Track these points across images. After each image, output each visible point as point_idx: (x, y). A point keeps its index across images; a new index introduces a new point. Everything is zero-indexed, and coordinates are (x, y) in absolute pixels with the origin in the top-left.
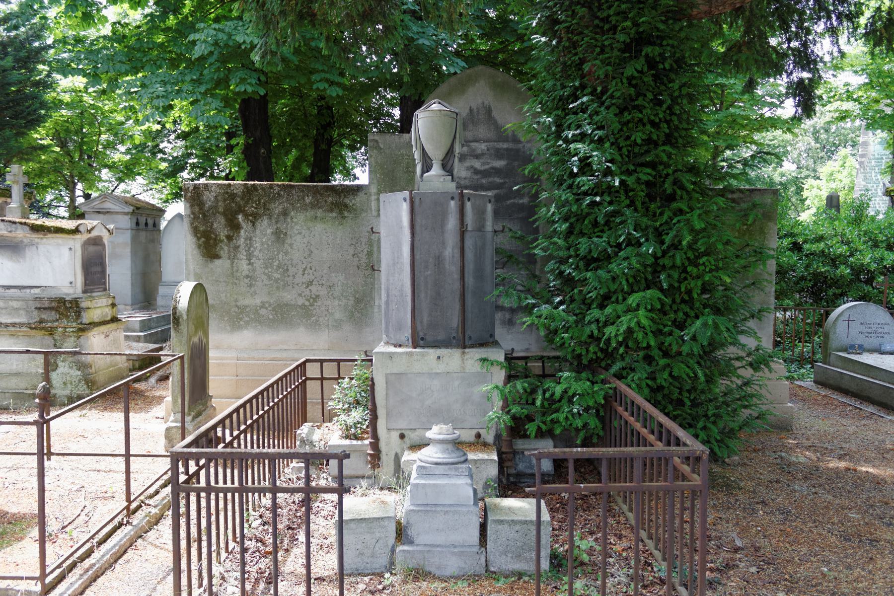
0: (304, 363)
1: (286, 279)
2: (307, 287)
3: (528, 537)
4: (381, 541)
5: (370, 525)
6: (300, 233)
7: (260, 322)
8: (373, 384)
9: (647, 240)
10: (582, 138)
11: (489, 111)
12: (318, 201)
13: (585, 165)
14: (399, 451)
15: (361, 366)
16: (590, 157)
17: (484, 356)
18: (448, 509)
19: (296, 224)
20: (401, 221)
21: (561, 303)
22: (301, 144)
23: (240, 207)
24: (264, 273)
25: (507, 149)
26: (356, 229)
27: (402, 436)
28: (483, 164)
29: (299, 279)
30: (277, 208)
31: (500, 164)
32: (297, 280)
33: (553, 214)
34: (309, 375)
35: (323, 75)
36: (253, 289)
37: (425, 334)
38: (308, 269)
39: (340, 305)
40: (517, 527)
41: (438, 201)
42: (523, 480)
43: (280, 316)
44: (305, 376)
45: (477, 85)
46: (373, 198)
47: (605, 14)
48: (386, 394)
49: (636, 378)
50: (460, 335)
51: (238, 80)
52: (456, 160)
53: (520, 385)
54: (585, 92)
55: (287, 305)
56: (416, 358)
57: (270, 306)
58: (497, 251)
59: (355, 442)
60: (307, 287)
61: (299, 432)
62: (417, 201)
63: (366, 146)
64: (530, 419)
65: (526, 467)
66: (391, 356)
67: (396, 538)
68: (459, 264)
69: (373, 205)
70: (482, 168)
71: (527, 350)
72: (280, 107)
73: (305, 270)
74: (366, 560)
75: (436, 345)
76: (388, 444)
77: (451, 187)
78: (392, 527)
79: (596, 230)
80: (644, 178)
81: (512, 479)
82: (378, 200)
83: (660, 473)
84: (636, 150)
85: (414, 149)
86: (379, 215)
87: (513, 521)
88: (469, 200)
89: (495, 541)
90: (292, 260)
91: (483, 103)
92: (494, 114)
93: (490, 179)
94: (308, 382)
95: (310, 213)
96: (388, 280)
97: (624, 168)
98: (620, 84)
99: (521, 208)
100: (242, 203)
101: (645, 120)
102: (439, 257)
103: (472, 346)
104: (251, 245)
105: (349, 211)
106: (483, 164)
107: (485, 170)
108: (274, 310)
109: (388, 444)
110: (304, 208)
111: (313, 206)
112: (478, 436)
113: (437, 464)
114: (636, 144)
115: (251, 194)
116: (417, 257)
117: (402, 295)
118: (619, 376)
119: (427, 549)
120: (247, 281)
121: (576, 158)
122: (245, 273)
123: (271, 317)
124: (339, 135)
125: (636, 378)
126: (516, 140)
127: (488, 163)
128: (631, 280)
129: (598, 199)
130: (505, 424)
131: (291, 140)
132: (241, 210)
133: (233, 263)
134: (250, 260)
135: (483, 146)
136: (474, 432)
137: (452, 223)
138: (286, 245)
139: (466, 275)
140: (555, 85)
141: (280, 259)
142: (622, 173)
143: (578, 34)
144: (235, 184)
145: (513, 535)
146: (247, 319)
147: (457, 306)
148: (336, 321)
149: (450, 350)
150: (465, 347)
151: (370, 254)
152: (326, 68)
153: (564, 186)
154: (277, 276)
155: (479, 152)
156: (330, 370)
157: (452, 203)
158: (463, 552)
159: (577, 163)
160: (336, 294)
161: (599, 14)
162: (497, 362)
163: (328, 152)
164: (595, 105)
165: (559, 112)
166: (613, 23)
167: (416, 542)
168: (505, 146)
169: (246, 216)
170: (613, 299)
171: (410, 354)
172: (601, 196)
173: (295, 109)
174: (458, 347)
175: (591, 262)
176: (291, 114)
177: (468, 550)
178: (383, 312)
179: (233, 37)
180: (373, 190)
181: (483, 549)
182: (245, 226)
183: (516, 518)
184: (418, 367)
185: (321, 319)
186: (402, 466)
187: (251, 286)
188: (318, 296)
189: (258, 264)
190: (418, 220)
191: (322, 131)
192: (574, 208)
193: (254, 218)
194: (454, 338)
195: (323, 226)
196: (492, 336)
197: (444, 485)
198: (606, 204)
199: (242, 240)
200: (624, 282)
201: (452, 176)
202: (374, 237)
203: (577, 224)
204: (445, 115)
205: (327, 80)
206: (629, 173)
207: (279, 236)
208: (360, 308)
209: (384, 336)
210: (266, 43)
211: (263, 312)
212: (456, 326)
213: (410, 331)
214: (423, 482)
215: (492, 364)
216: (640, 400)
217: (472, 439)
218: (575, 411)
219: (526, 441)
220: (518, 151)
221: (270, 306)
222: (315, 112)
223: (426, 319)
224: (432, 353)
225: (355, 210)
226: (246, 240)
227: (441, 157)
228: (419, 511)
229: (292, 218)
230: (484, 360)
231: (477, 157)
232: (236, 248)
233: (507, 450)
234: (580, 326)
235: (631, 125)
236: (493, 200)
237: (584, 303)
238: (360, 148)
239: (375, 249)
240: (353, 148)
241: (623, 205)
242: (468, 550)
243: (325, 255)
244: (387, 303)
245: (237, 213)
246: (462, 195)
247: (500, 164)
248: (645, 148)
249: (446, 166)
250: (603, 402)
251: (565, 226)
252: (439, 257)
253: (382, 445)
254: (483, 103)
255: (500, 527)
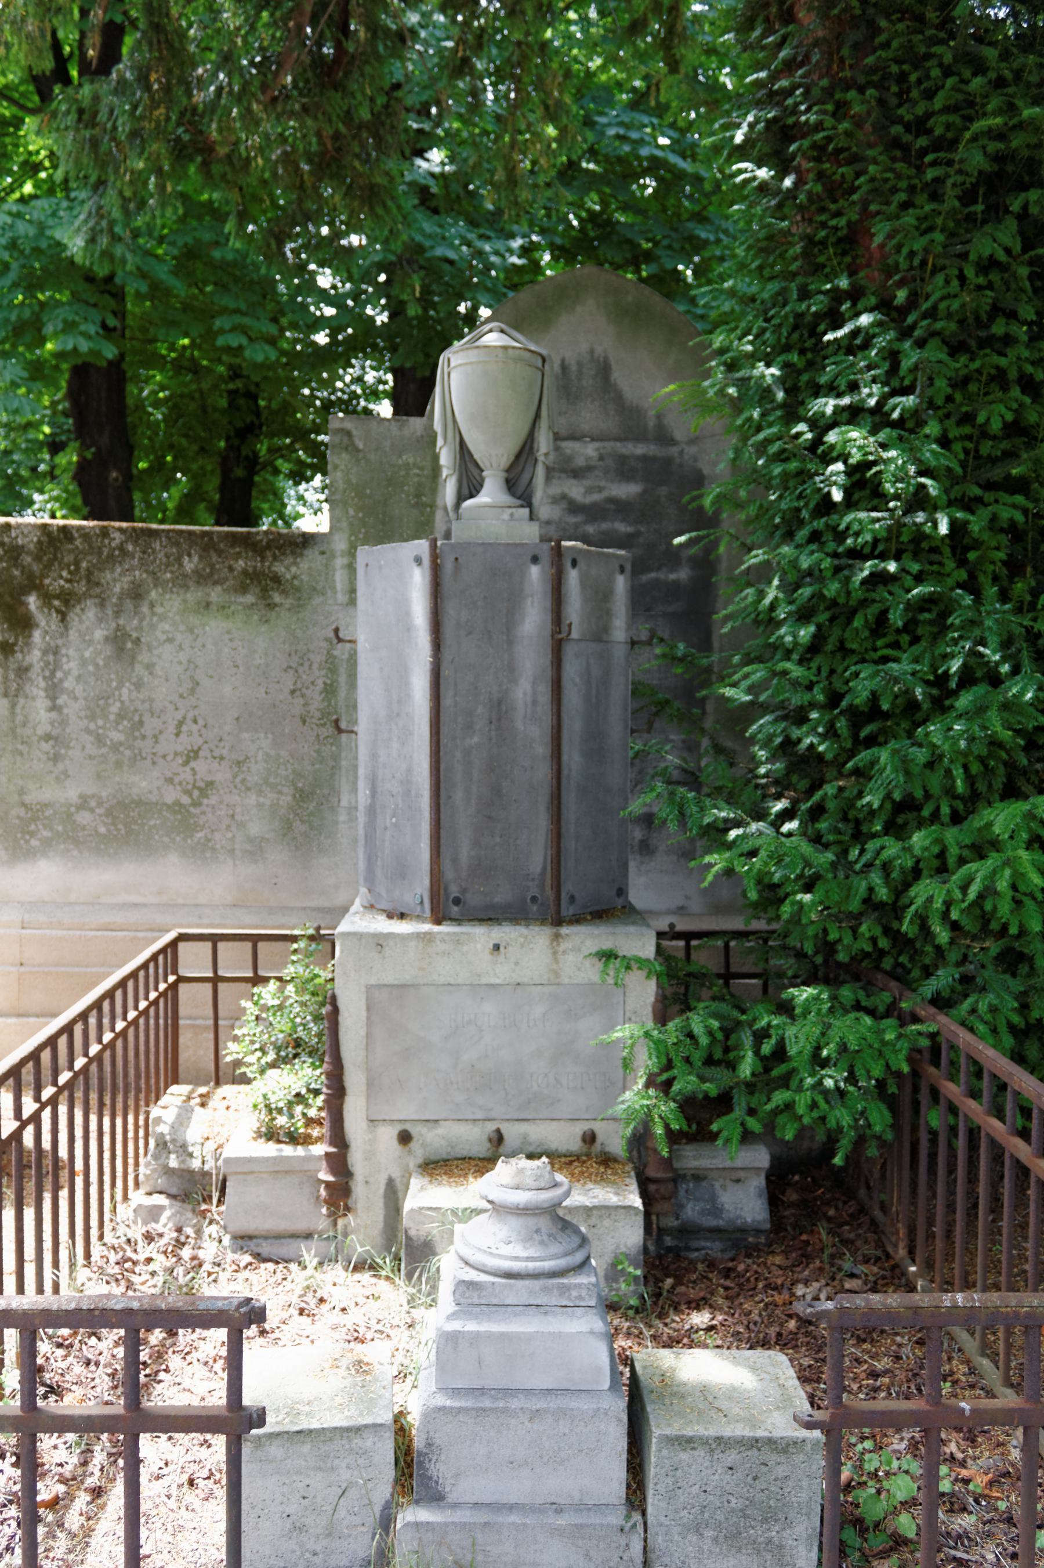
0: (174, 944)
1: (139, 743)
2: (186, 763)
3: (760, 1485)
4: (353, 1493)
5: (324, 1448)
6: (170, 640)
7: (76, 842)
8: (336, 1010)
9: (1016, 671)
10: (853, 415)
11: (604, 370)
12: (212, 566)
13: (864, 485)
14: (396, 1174)
16: (875, 463)
17: (607, 945)
18: (541, 1404)
19: (163, 618)
21: (787, 815)
22: (194, 466)
23: (31, 576)
24: (88, 731)
25: (644, 458)
27: (405, 1138)
28: (589, 490)
29: (168, 744)
30: (117, 581)
31: (626, 490)
32: (160, 749)
33: (773, 607)
34: (184, 972)
35: (238, 319)
36: (61, 766)
37: (464, 891)
38: (189, 721)
39: (260, 806)
40: (732, 1457)
41: (500, 566)
42: (695, 1244)
43: (126, 827)
44: (175, 971)
45: (579, 309)
46: (340, 562)
47: (920, 110)
48: (368, 1035)
49: (983, 1007)
50: (550, 893)
51: (60, 326)
53: (700, 1023)
54: (860, 306)
55: (139, 803)
56: (442, 947)
57: (100, 804)
59: (288, 1150)
60: (186, 763)
61: (155, 1112)
62: (448, 566)
64: (723, 1103)
65: (702, 1213)
66: (379, 941)
67: (396, 1481)
68: (548, 719)
69: (340, 578)
71: (681, 911)
72: (152, 390)
73: (181, 723)
74: (311, 1545)
75: (489, 916)
76: (369, 1156)
78: (385, 1450)
79: (879, 643)
80: (1006, 514)
81: (668, 1241)
82: (351, 568)
83: (1024, 1226)
84: (986, 448)
85: (440, 442)
86: (352, 602)
87: (719, 1439)
88: (574, 563)
89: (670, 1497)
90: (152, 700)
91: (592, 352)
92: (616, 376)
93: (605, 526)
94: (183, 988)
95: (194, 595)
96: (374, 756)
97: (956, 492)
98: (955, 283)
99: (674, 590)
100: (36, 568)
101: (1013, 374)
102: (500, 703)
103: (577, 920)
104: (57, 666)
105: (284, 593)
106: (589, 490)
107: (594, 505)
108: (109, 813)
109: (369, 1156)
110: (182, 582)
111: (203, 578)
112: (590, 1138)
113: (509, 1275)
114: (984, 434)
115: (56, 549)
116: (447, 701)
117: (407, 793)
118: (941, 1003)
119: (480, 1517)
120: (46, 746)
121: (839, 466)
122: (44, 728)
123: (102, 830)
124: (270, 450)
125: (983, 1007)
128: (975, 768)
129: (892, 567)
130: (667, 1126)
131: (175, 458)
132: (33, 584)
133: (13, 705)
134: (53, 699)
135: (589, 451)
136: (579, 1129)
137: (533, 619)
138: (138, 668)
141: (125, 697)
142: (950, 504)
143: (849, 162)
144: (19, 526)
145: (719, 1478)
146: (46, 834)
147: (543, 822)
148: (251, 840)
149: (522, 930)
150: (558, 921)
151: (330, 690)
152: (243, 307)
154: (116, 736)
155: (580, 462)
156: (234, 961)
157: (535, 571)
158: (581, 1526)
159: (841, 479)
160: (253, 779)
161: (901, 111)
163: (248, 484)
164: (891, 335)
165: (794, 357)
166: (938, 131)
167: (451, 1498)
168: (640, 450)
169: (46, 598)
170: (926, 813)
171: (426, 938)
172: (897, 558)
173: (182, 396)
174: (543, 922)
175: (870, 723)
176: (175, 406)
177: (595, 1519)
178: (361, 832)
179: (48, 233)
180: (340, 544)
181: (637, 1517)
182: (45, 621)
183: (727, 1432)
185: (217, 836)
186: (406, 1222)
187: (56, 758)
188: (210, 784)
189: (73, 709)
191: (236, 442)
192: (832, 589)
193: (64, 604)
194: (534, 899)
195: (224, 625)
196: (621, 892)
197: (530, 1337)
198: (908, 580)
199: (36, 654)
200: (958, 772)
202: (341, 651)
203: (841, 626)
204: (516, 360)
205: (244, 330)
206: (969, 505)
207: (123, 646)
208: (307, 810)
209: (363, 890)
210: (100, 208)
211: (84, 818)
213: (427, 882)
214: (472, 1326)
215: (628, 968)
216: (995, 1059)
217: (575, 1145)
218: (829, 1083)
219: (704, 1149)
220: (668, 461)
221: (100, 804)
222: (223, 403)
223: (465, 852)
224: (480, 936)
225: (298, 590)
226: (45, 652)
227: (505, 461)
228: (460, 1410)
229: (152, 606)
230: (608, 956)
231: (576, 474)
232: (23, 671)
233: (660, 1175)
234: (841, 875)
235: (973, 387)
236: (628, 567)
237: (845, 819)
238: (312, 478)
239: (342, 679)
241: (950, 582)
242: (595, 1519)
243: (227, 690)
244: (372, 811)
245: (25, 590)
248: (1005, 445)
249: (517, 484)
250: (906, 1069)
251: (805, 633)
253: (356, 1159)
254: (592, 352)
255: (684, 1456)
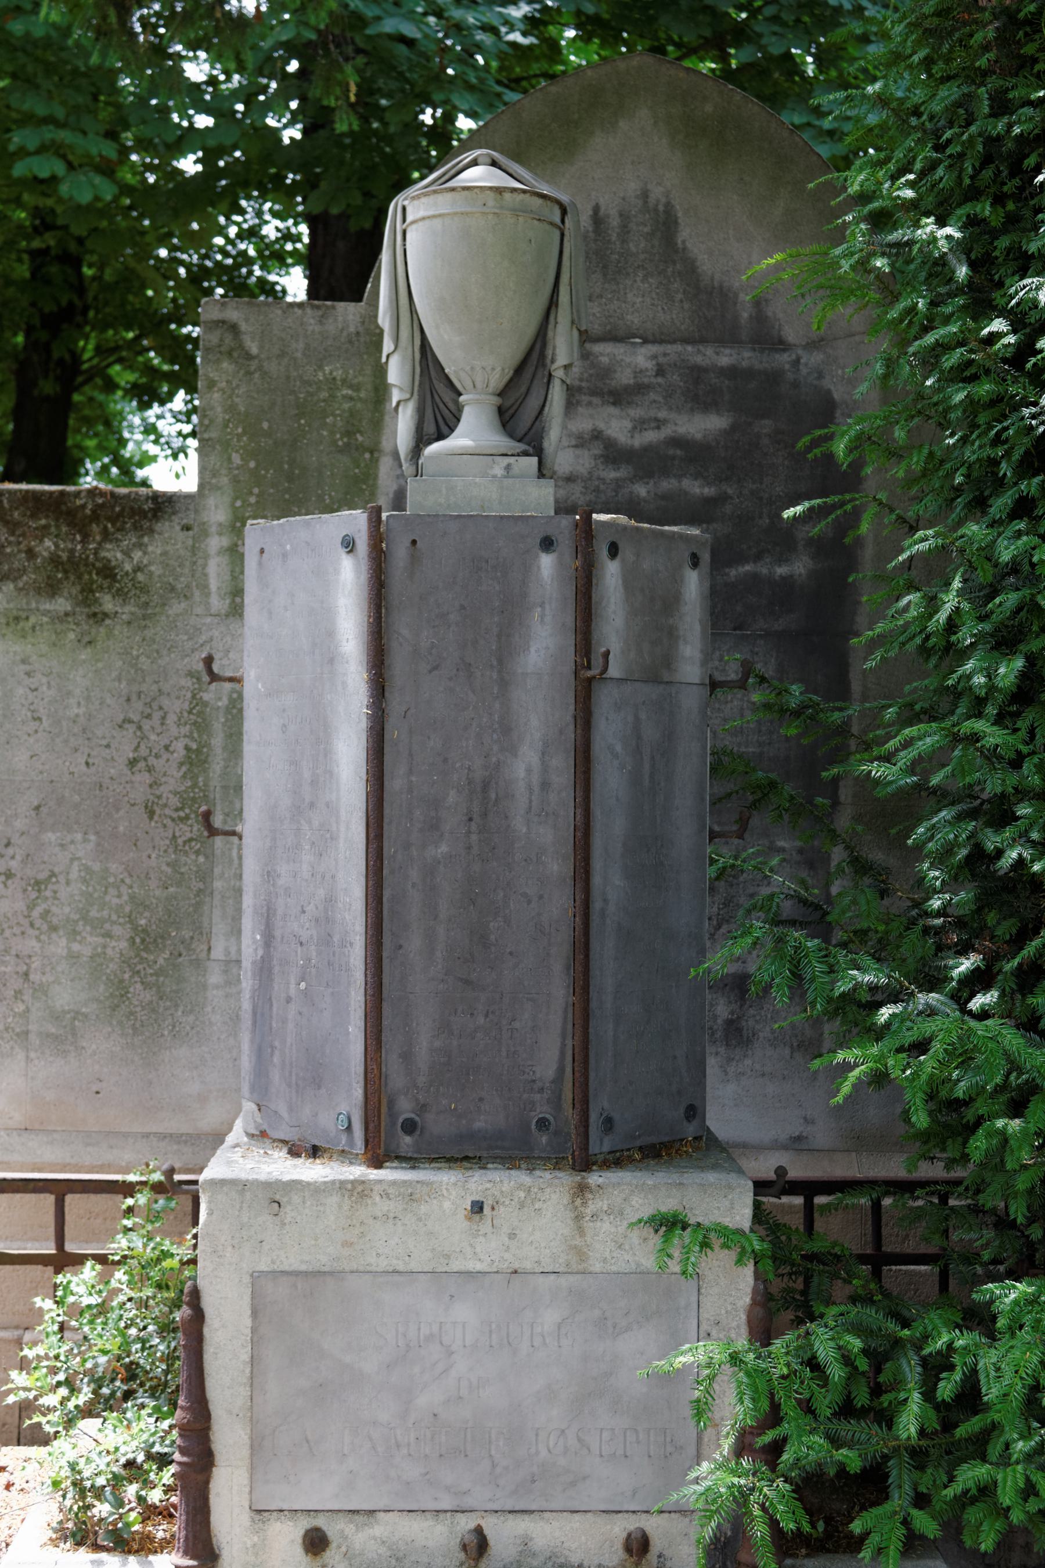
8: (198, 1316)
11: (666, 224)
15: (152, 1216)
17: (668, 1204)
20: (331, 633)
21: (978, 981)
25: (732, 372)
26: (144, 663)
28: (640, 425)
31: (702, 425)
33: (952, 626)
35: (49, 133)
37: (423, 1108)
39: (73, 957)
41: (488, 552)
46: (215, 543)
50: (569, 1113)
52: (557, 395)
56: (382, 1206)
58: (720, 765)
62: (400, 553)
63: (191, 390)
66: (275, 1196)
68: (567, 815)
69: (215, 570)
70: (638, 441)
77: (538, 498)
82: (235, 554)
85: (388, 345)
86: (236, 610)
88: (614, 551)
91: (645, 195)
92: (685, 235)
93: (668, 485)
96: (269, 875)
99: (784, 592)
102: (486, 786)
105: (121, 594)
106: (640, 425)
107: (647, 449)
116: (395, 783)
117: (326, 941)
124: (99, 350)
126: (767, 339)
127: (659, 424)
130: (774, 1524)
135: (641, 358)
136: (620, 1528)
137: (543, 645)
139: (597, 864)
140: (969, 97)
147: (558, 991)
148: (56, 1017)
149: (521, 1177)
151: (196, 760)
152: (60, 113)
153: (1001, 504)
155: (624, 378)
157: (546, 562)
160: (61, 912)
162: (723, 1231)
163: (62, 406)
165: (985, 209)
168: (725, 358)
171: (357, 1190)
174: (557, 1164)
180: (217, 513)
184: (388, 1245)
190: (403, 628)
191: (43, 336)
195: (18, 648)
196: (694, 1112)
201: (538, 452)
202: (216, 695)
204: (516, 211)
205: (59, 150)
209: (249, 1106)
212: (550, 1073)
213: (358, 1093)
215: (705, 1245)
220: (774, 377)
225: (144, 589)
227: (497, 379)
230: (669, 1224)
231: (619, 397)
236: (706, 557)
238: (170, 396)
239: (218, 741)
240: (148, 394)
244: (264, 969)
246: (586, 531)
247: (702, 425)
249: (517, 416)
252: (486, 786)
254: (645, 195)
